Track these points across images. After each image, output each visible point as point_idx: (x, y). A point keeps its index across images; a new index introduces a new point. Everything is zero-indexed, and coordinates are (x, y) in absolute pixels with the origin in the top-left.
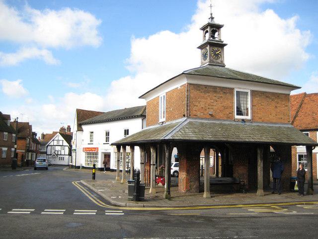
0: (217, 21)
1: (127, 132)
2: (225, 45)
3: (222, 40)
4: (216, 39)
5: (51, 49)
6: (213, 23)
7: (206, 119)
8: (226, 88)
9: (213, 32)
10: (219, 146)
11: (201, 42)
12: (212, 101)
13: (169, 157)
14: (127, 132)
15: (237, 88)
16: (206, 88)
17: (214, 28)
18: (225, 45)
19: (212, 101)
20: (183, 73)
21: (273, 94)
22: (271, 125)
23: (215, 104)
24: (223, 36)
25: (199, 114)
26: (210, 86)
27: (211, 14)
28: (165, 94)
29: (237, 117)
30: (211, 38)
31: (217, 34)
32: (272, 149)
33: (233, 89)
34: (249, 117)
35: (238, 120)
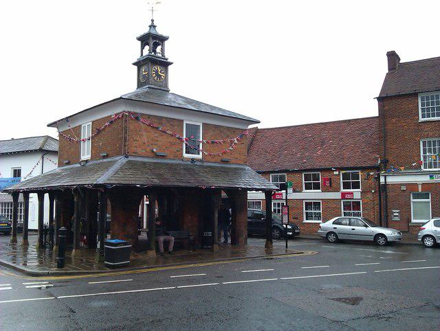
0: (160, 31)
1: (17, 173)
2: (171, 64)
3: (166, 57)
4: (159, 55)
5: (143, 48)
6: (153, 32)
7: (147, 157)
8: (174, 119)
9: (156, 45)
10: (157, 192)
11: (136, 56)
12: (157, 135)
13: (350, 244)
14: (17, 173)
15: (188, 121)
16: (149, 118)
17: (158, 40)
18: (171, 64)
19: (157, 135)
20: (121, 98)
21: (228, 128)
22: (236, 167)
23: (160, 139)
24: (170, 51)
25: (140, 151)
26: (155, 116)
27: (152, 21)
28: (91, 123)
29: (186, 155)
30: (153, 53)
31: (159, 49)
32: (224, 195)
33: (182, 121)
34: (200, 156)
35: (188, 159)
